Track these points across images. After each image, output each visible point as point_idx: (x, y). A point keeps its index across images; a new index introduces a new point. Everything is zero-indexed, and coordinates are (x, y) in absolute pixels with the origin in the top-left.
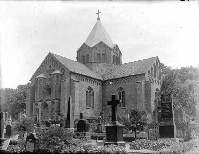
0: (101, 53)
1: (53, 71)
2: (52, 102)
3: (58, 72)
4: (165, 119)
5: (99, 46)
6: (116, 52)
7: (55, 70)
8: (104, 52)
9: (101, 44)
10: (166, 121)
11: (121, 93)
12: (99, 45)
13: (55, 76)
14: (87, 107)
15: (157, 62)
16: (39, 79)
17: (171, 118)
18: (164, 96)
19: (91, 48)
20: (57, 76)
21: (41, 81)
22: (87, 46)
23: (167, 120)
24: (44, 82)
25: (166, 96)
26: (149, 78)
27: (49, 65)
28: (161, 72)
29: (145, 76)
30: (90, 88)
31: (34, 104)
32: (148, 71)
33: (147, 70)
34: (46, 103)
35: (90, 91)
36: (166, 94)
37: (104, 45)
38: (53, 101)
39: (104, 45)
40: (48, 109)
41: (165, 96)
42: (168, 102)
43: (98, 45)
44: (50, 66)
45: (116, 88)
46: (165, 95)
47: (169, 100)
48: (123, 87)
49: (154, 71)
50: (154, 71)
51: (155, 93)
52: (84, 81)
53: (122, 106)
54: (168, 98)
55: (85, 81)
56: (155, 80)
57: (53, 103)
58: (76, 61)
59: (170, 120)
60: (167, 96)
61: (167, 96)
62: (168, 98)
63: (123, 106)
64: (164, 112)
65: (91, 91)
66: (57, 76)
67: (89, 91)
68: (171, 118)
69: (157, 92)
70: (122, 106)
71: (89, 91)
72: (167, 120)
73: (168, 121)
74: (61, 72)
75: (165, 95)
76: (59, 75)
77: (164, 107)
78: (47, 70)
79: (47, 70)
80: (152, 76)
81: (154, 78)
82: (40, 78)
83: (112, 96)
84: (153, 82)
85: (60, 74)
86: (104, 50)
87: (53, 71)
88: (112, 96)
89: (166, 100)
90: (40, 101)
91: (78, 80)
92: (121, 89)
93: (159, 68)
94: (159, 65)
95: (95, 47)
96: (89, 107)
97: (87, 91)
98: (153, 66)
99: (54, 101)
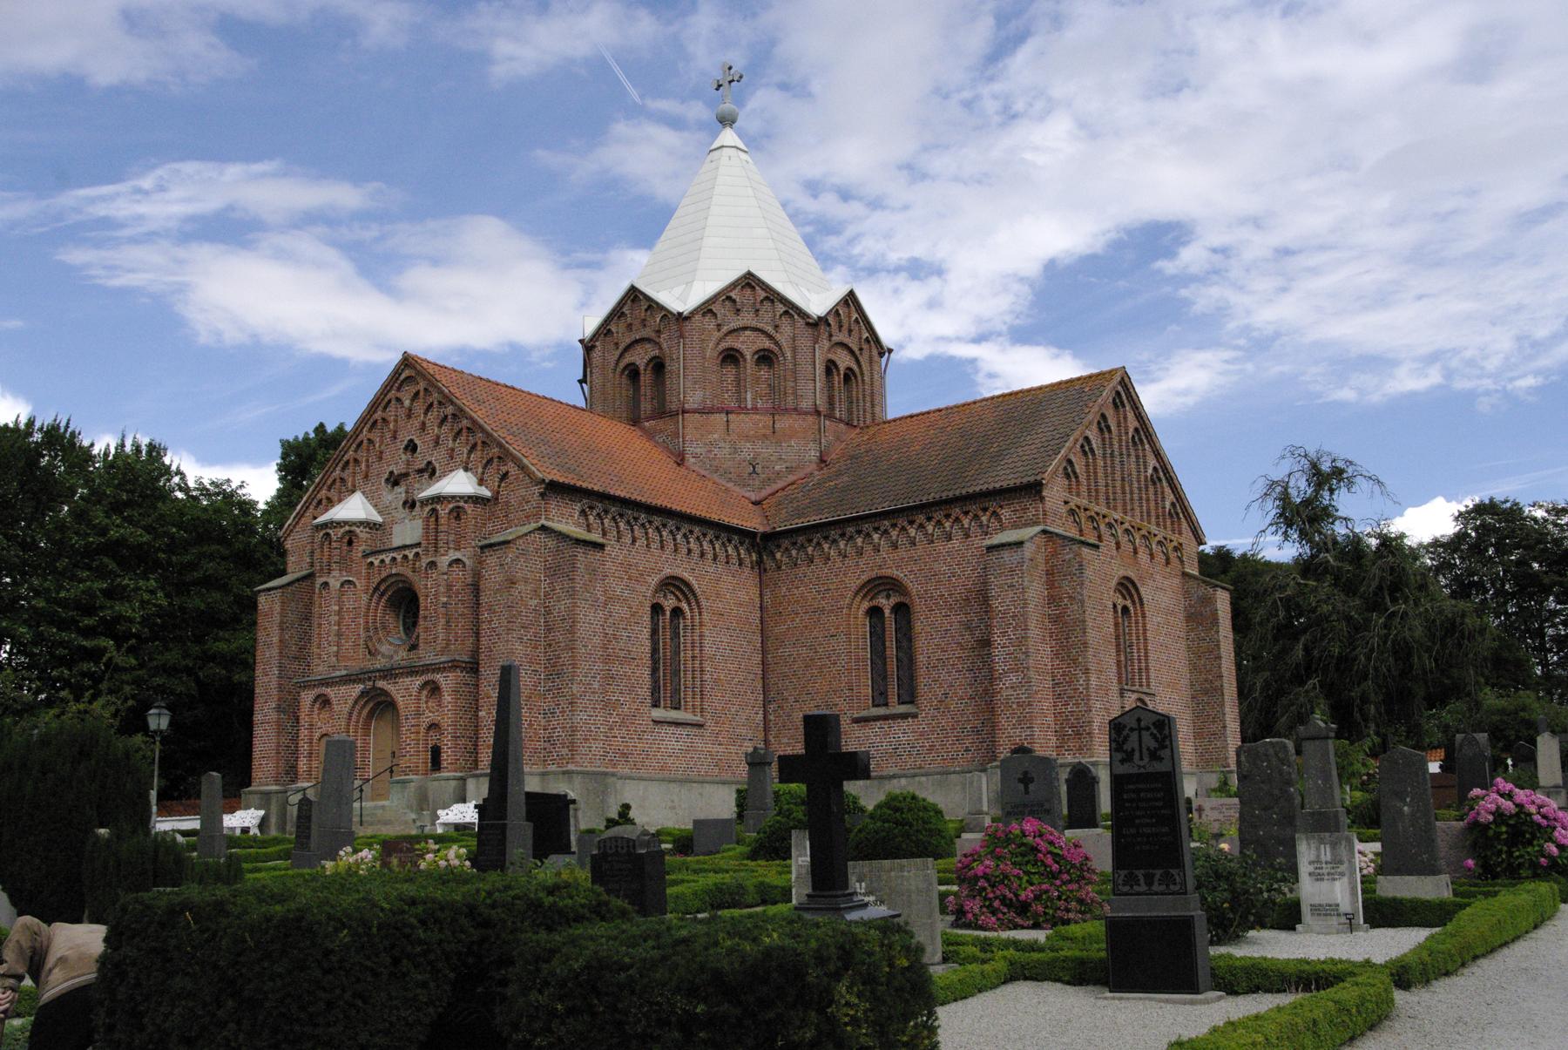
0: (748, 345)
1: (426, 475)
2: (426, 683)
3: (459, 483)
4: (1140, 873)
5: (734, 301)
6: (847, 340)
7: (444, 475)
8: (767, 344)
9: (748, 292)
10: (1143, 888)
11: (887, 612)
12: (733, 294)
13: (443, 511)
14: (658, 713)
15: (1117, 403)
16: (335, 534)
17: (1173, 871)
18: (1125, 733)
19: (680, 314)
20: (457, 513)
21: (350, 543)
22: (653, 306)
23: (1149, 883)
24: (366, 556)
25: (1140, 729)
26: (1072, 512)
27: (400, 436)
28: (1150, 471)
29: (1042, 499)
30: (673, 584)
31: (307, 697)
32: (1081, 441)
33: (1056, 462)
34: (384, 692)
35: (672, 606)
36: (1139, 720)
37: (763, 295)
38: (430, 677)
39: (767, 298)
40: (398, 734)
41: (1132, 730)
42: (1150, 770)
43: (725, 296)
44: (412, 447)
45: (854, 582)
46: (1134, 725)
47: (1161, 759)
48: (895, 573)
49: (1100, 463)
50: (1100, 463)
51: (1115, 611)
52: (634, 541)
53: (893, 699)
54: (1153, 744)
55: (642, 542)
56: (1110, 525)
57: (434, 689)
58: (581, 403)
59: (1168, 879)
60: (1148, 729)
61: (1148, 729)
62: (1153, 744)
63: (901, 703)
64: (1133, 831)
65: (685, 606)
66: (457, 513)
67: (669, 603)
68: (1173, 871)
69: (1128, 603)
70: (893, 699)
71: (669, 603)
72: (1149, 880)
73: (1156, 888)
74: (481, 482)
75: (1134, 725)
76: (469, 508)
77: (1131, 801)
78: (391, 473)
79: (391, 473)
80: (1093, 494)
81: (1104, 511)
82: (346, 523)
83: (809, 721)
84: (1100, 538)
85: (475, 499)
86: (770, 329)
87: (426, 475)
88: (809, 721)
89: (1137, 755)
90: (348, 679)
91: (595, 537)
92: (889, 585)
93: (1134, 443)
94: (1136, 424)
95: (706, 309)
96: (674, 715)
97: (657, 609)
98: (1095, 427)
99: (438, 677)
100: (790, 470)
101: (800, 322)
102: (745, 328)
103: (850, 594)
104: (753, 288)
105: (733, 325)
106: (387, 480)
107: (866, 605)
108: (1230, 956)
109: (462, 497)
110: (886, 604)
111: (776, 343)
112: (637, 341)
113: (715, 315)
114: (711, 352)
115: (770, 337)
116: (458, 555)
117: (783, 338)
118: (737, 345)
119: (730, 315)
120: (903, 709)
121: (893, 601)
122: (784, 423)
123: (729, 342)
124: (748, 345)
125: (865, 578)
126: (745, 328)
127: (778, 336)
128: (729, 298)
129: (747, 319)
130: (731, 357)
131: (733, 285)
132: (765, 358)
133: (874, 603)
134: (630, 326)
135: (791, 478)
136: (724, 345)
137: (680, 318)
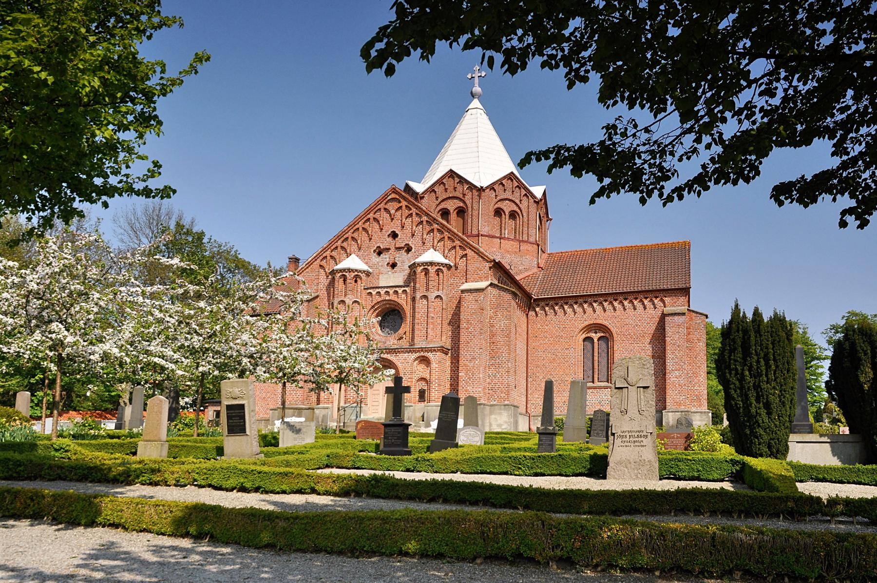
0: (507, 207)
5: (503, 185)
8: (462, 204)
11: (596, 340)
12: (503, 182)
13: (432, 270)
95: (491, 187)
100: (526, 270)
101: (532, 200)
102: (506, 199)
103: (578, 330)
104: (453, 178)
105: (503, 197)
106: (375, 251)
107: (584, 336)
108: (393, 478)
109: (426, 263)
110: (595, 336)
111: (520, 208)
112: (449, 198)
113: (495, 191)
114: (492, 209)
115: (461, 200)
116: (439, 293)
117: (524, 206)
118: (502, 207)
119: (502, 192)
120: (606, 384)
121: (599, 335)
122: (524, 247)
123: (499, 205)
124: (507, 207)
125: (587, 323)
126: (506, 199)
127: (520, 205)
128: (502, 184)
129: (508, 195)
130: (498, 212)
131: (504, 177)
132: (513, 215)
133: (589, 335)
134: (446, 190)
135: (527, 274)
136: (497, 206)
137: (481, 190)
